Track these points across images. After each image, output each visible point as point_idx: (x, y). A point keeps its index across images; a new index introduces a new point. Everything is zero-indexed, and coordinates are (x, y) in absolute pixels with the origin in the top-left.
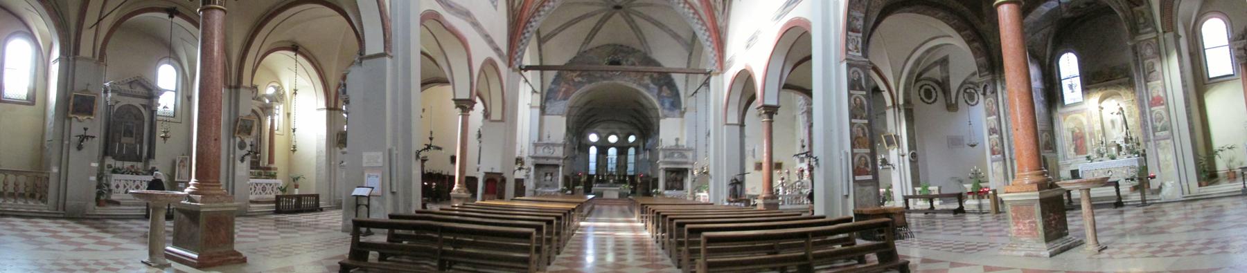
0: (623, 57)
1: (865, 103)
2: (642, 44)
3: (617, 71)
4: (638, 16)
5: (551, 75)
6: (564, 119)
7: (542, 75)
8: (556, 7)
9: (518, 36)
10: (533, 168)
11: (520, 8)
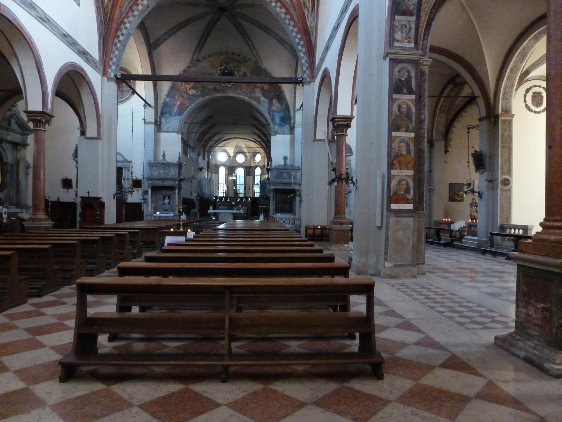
0: (234, 67)
1: (413, 110)
3: (229, 82)
5: (165, 86)
6: (179, 137)
7: (155, 86)
10: (150, 191)
11: (110, 5)
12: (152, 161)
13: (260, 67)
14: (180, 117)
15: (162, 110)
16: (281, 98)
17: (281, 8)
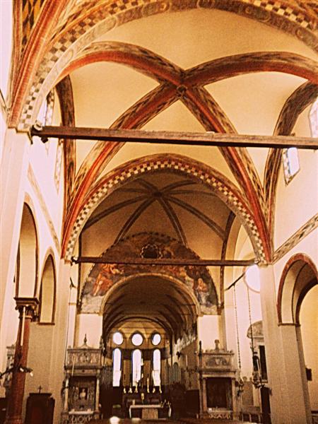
0: (158, 246)
2: (178, 232)
4: (176, 203)
6: (102, 317)
8: (108, 194)
9: (72, 223)
11: (76, 193)
12: (72, 347)
13: (184, 247)
14: (102, 297)
15: (83, 290)
16: (207, 278)
17: (233, 196)
